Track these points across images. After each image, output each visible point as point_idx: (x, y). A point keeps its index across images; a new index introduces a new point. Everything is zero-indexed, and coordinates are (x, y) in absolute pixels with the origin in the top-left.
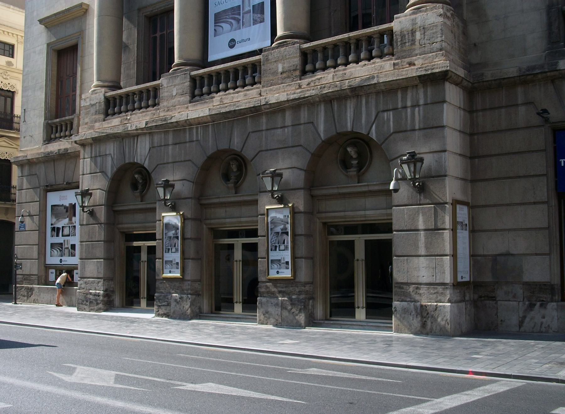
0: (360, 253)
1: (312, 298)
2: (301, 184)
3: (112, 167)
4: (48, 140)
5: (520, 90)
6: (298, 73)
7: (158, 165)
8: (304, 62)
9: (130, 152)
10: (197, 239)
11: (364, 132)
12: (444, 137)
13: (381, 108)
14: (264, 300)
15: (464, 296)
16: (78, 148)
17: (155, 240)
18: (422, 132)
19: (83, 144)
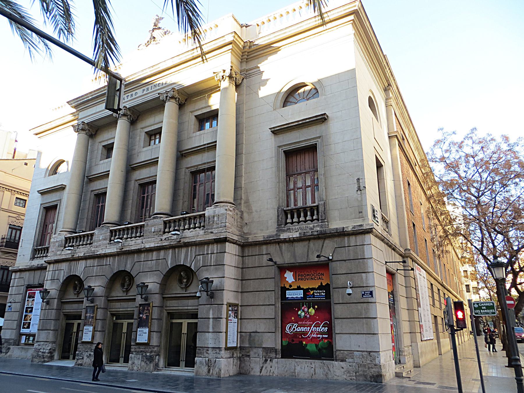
0: (185, 330)
1: (159, 355)
2: (157, 291)
3: (63, 277)
4: (33, 258)
5: (264, 247)
6: (161, 233)
8: (66, 243)
9: (74, 269)
10: (104, 320)
11: (189, 265)
12: (224, 270)
14: (133, 355)
15: (233, 354)
16: (46, 264)
17: (81, 319)
19: (49, 263)
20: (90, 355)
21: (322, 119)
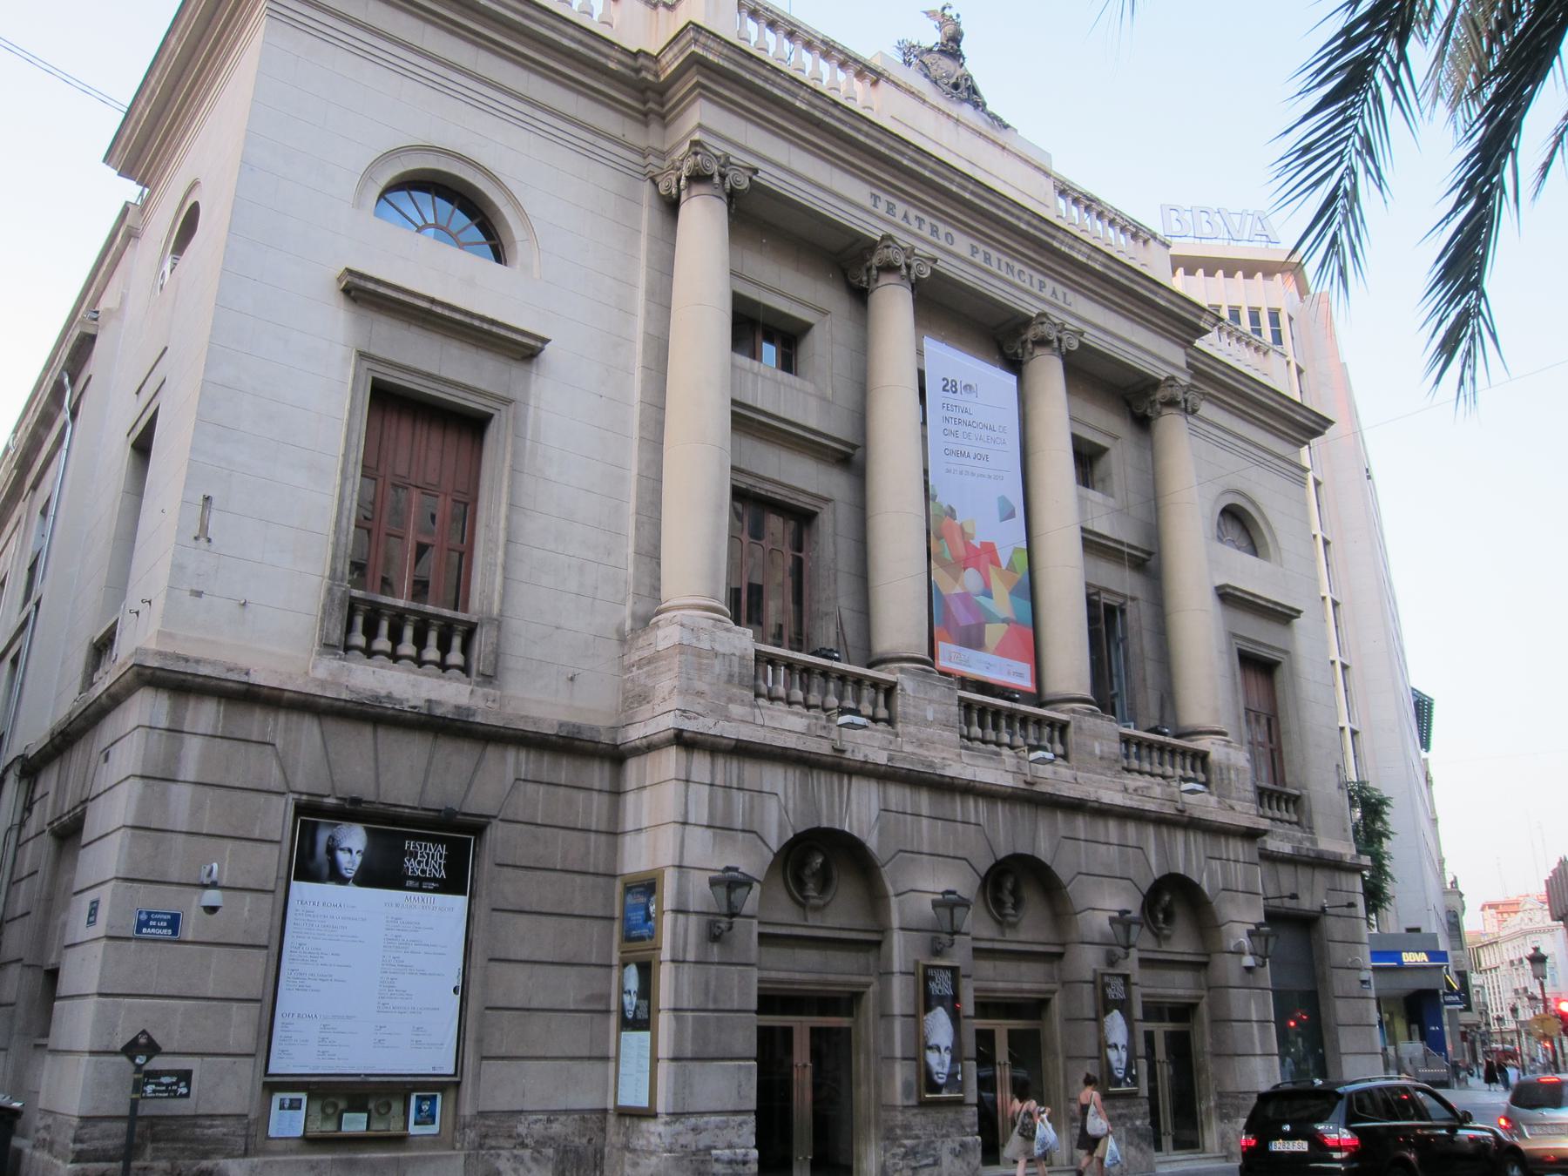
3: (781, 826)
20: (963, 1145)
21: (522, 350)
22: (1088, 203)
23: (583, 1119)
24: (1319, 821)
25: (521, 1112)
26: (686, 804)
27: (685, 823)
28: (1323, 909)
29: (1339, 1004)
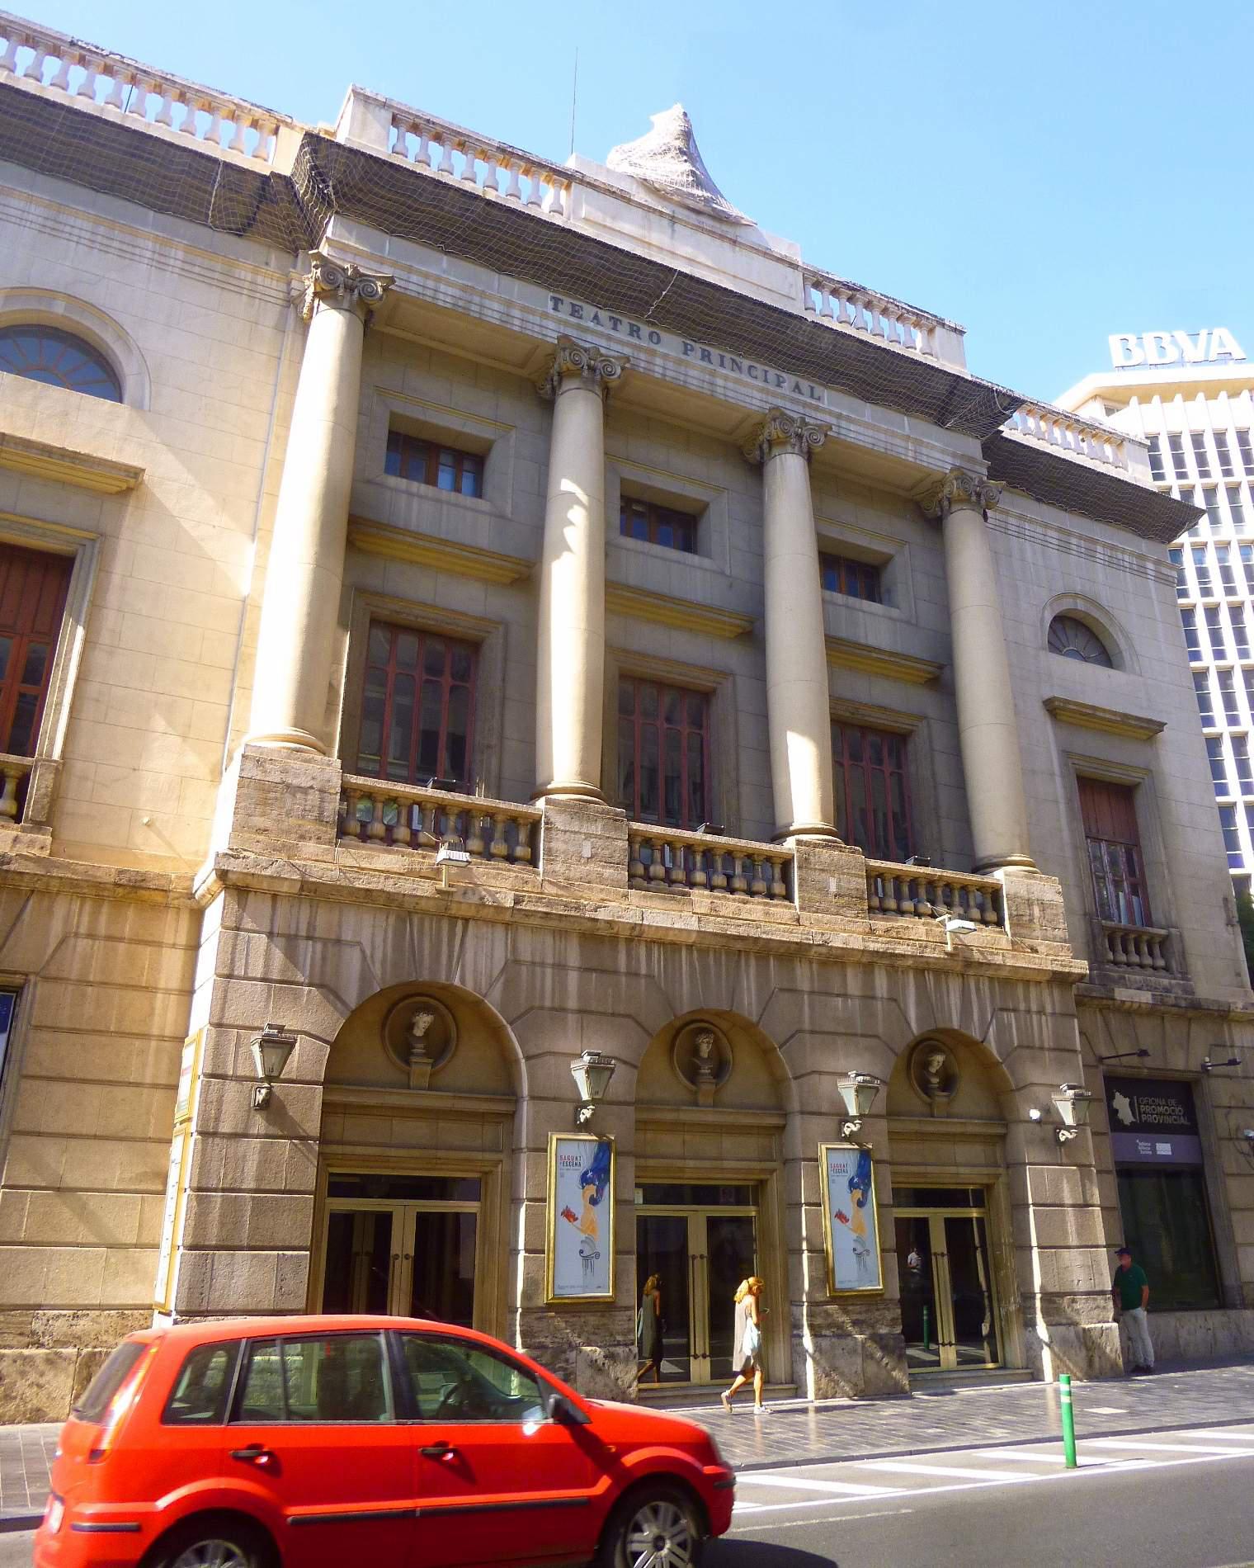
0: (403, 1240)
7: (532, 1008)
13: (999, 1004)
18: (1053, 1054)
22: (852, 293)
23: (123, 1316)
24: (1197, 965)
25: (39, 1307)
26: (233, 953)
27: (230, 976)
28: (1204, 1067)
29: (1232, 1183)
